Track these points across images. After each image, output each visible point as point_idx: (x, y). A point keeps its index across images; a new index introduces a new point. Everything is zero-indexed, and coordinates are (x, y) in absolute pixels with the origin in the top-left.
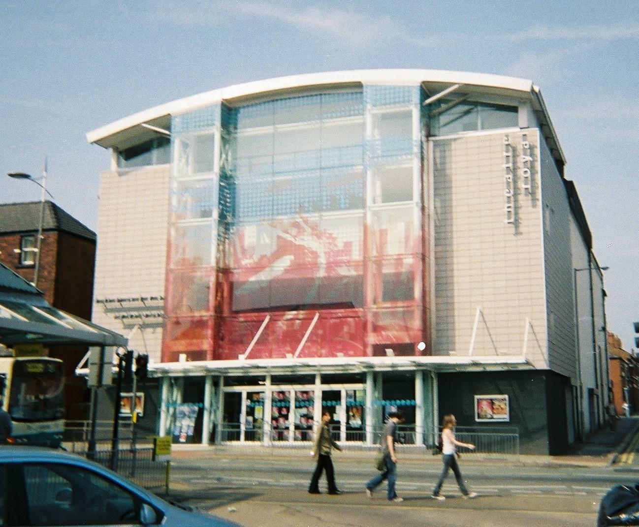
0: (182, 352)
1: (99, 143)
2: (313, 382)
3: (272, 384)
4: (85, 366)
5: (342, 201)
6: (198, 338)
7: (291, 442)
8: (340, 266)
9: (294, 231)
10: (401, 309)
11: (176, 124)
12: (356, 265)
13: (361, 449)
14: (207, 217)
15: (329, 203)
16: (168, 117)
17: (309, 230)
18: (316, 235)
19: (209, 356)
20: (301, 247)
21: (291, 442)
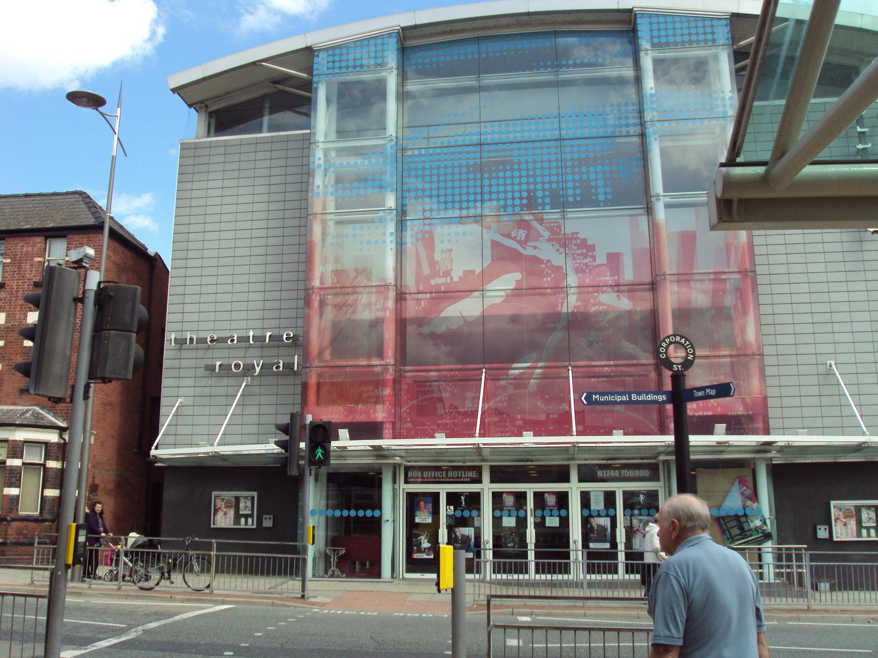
0: (343, 425)
1: (181, 92)
2: (567, 480)
3: (491, 482)
4: (157, 448)
5: (601, 190)
6: (366, 401)
7: (531, 575)
8: (603, 292)
9: (522, 234)
10: (728, 360)
11: (321, 63)
12: (632, 289)
13: (519, 584)
14: (841, 67)
15: (578, 191)
16: (309, 51)
17: (546, 234)
18: (558, 241)
19: (387, 431)
20: (536, 260)
21: (531, 575)
